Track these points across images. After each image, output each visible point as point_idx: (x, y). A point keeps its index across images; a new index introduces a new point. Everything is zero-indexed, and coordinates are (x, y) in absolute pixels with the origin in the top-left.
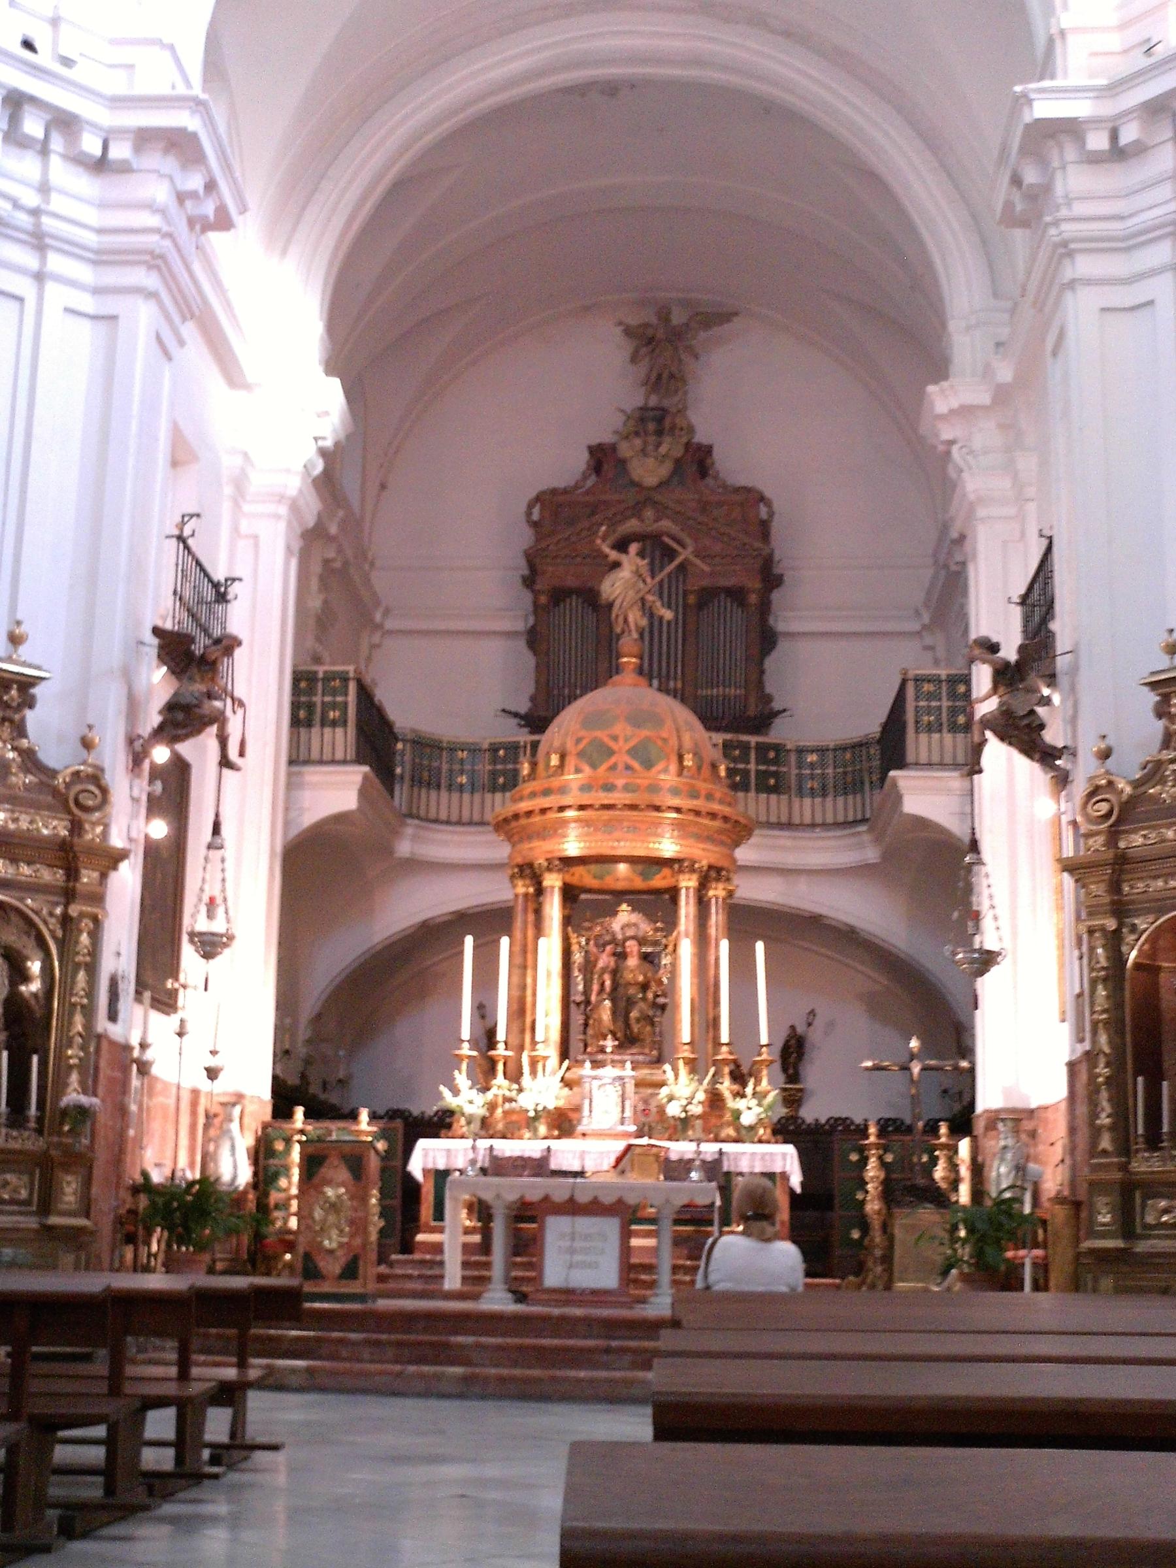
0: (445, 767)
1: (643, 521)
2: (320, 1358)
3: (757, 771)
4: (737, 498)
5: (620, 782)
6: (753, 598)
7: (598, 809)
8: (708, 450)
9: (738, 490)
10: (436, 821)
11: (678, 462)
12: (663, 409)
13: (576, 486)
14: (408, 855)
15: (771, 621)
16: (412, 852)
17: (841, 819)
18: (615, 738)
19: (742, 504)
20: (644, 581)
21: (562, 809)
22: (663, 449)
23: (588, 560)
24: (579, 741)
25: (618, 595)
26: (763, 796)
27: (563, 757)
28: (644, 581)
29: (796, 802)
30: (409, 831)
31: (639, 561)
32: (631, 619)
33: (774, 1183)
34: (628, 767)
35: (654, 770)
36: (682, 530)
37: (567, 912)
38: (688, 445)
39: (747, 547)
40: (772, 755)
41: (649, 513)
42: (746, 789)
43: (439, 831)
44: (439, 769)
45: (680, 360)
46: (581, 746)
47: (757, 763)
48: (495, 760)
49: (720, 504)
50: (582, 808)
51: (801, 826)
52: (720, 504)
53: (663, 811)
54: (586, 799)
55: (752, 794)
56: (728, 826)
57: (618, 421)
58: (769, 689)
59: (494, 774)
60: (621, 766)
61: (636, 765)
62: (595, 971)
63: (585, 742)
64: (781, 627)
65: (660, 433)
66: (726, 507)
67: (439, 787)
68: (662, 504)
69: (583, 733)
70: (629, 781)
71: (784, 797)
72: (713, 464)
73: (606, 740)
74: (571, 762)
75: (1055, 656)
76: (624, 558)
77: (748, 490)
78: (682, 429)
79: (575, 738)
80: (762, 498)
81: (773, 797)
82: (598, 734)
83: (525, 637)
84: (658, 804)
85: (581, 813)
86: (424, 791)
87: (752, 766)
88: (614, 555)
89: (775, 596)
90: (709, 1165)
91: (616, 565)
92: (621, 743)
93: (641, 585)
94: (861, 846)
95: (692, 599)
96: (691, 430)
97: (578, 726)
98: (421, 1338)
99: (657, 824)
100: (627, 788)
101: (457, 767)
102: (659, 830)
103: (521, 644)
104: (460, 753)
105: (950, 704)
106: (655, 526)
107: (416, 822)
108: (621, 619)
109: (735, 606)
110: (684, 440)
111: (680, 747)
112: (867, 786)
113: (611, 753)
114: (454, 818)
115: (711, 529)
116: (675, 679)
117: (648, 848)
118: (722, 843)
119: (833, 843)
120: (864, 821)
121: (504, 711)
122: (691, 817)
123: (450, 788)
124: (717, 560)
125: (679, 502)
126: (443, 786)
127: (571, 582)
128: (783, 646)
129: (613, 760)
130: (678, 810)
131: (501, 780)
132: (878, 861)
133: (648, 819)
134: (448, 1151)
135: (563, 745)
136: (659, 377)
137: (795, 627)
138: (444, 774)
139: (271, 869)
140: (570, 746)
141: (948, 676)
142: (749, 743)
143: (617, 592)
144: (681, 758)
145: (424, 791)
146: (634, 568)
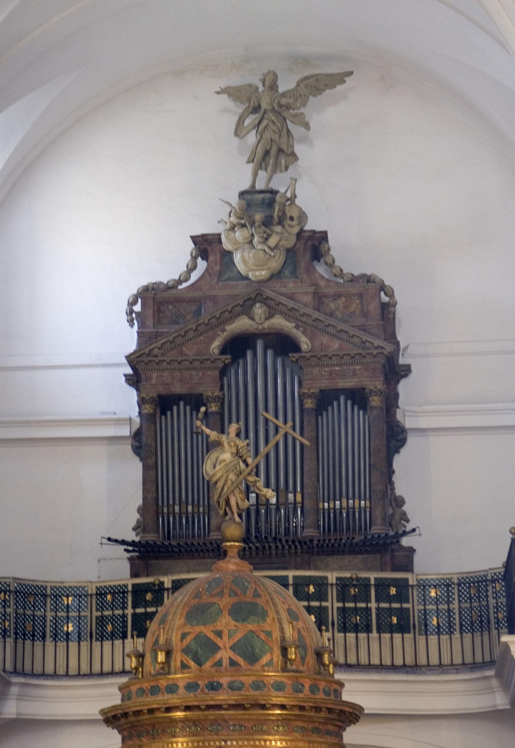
0: (50, 615)
1: (253, 319)
2: (301, 517)
3: (378, 609)
4: (354, 289)
5: (225, 681)
6: (375, 401)
7: (205, 710)
8: (323, 236)
9: (353, 279)
10: (43, 675)
11: (290, 252)
12: (274, 192)
13: (180, 282)
14: (14, 716)
15: (399, 416)
16: (18, 714)
17: (469, 659)
18: (219, 634)
19: (360, 295)
20: (245, 462)
21: (169, 709)
22: (273, 241)
23: (196, 364)
24: (184, 636)
25: (219, 480)
26: (386, 636)
27: (168, 654)
28: (245, 462)
29: (421, 640)
30: (14, 690)
31: (241, 443)
32: (233, 502)
33: (188, 633)
34: (233, 663)
35: (257, 667)
36: (297, 327)
37: (141, 606)
38: (300, 235)
39: (367, 344)
40: (393, 591)
41: (259, 310)
42: (368, 629)
43: (490, 707)
44: (44, 617)
45: (288, 131)
46: (186, 642)
47: (377, 601)
48: (101, 607)
49: (337, 296)
50: (188, 708)
51: (429, 668)
52: (337, 296)
53: (267, 709)
54: (191, 699)
55: (374, 634)
56: (334, 716)
57: (224, 212)
58: (400, 490)
59: (101, 621)
60: (226, 662)
61: (241, 661)
62: (243, 273)
63: (189, 638)
64: (409, 423)
65: (267, 222)
66: (343, 299)
67: (44, 637)
68: (274, 300)
69: (186, 630)
70: (233, 679)
71: (408, 636)
72: (329, 249)
73: (211, 636)
74: (178, 658)
75: (345, 632)
76: (224, 438)
77: (368, 279)
78: (292, 218)
79: (180, 633)
80: (383, 287)
81: (397, 636)
82: (202, 629)
83: (130, 442)
84: (263, 702)
85: (188, 713)
86: (28, 642)
87: (373, 605)
88: (213, 435)
89: (403, 387)
90: (129, 378)
91: (218, 444)
92: (225, 638)
93: (242, 466)
94: (491, 690)
95: (309, 404)
96: (303, 217)
97: (182, 620)
98: (322, 522)
99: (265, 721)
100: (232, 687)
101: (62, 614)
102: (153, 404)
103: (128, 448)
104: (65, 599)
105: (341, 605)
106: (267, 324)
107: (21, 680)
108: (223, 503)
109: (356, 408)
110: (296, 230)
111: (283, 639)
112: (493, 626)
113: (216, 648)
114: (434, 660)
115: (327, 326)
116: (295, 492)
117: (168, 679)
118: (329, 733)
119: (462, 686)
120: (492, 663)
121: (109, 539)
122: (296, 712)
123: (55, 637)
124: (335, 361)
125: (292, 297)
126: (48, 634)
127: (178, 389)
128: (411, 441)
129: (218, 656)
130: (283, 707)
131: (110, 628)
132: (509, 707)
133: (254, 717)
134: (318, 310)
135: (168, 641)
136: (267, 153)
137: (424, 423)
138: (48, 624)
139: (481, 708)
140: (176, 644)
141: (371, 608)
142: (287, 577)
143: (219, 475)
144: (284, 650)
145: (28, 642)
146: (234, 450)
